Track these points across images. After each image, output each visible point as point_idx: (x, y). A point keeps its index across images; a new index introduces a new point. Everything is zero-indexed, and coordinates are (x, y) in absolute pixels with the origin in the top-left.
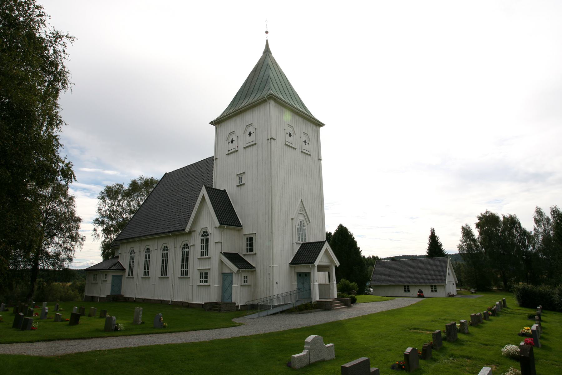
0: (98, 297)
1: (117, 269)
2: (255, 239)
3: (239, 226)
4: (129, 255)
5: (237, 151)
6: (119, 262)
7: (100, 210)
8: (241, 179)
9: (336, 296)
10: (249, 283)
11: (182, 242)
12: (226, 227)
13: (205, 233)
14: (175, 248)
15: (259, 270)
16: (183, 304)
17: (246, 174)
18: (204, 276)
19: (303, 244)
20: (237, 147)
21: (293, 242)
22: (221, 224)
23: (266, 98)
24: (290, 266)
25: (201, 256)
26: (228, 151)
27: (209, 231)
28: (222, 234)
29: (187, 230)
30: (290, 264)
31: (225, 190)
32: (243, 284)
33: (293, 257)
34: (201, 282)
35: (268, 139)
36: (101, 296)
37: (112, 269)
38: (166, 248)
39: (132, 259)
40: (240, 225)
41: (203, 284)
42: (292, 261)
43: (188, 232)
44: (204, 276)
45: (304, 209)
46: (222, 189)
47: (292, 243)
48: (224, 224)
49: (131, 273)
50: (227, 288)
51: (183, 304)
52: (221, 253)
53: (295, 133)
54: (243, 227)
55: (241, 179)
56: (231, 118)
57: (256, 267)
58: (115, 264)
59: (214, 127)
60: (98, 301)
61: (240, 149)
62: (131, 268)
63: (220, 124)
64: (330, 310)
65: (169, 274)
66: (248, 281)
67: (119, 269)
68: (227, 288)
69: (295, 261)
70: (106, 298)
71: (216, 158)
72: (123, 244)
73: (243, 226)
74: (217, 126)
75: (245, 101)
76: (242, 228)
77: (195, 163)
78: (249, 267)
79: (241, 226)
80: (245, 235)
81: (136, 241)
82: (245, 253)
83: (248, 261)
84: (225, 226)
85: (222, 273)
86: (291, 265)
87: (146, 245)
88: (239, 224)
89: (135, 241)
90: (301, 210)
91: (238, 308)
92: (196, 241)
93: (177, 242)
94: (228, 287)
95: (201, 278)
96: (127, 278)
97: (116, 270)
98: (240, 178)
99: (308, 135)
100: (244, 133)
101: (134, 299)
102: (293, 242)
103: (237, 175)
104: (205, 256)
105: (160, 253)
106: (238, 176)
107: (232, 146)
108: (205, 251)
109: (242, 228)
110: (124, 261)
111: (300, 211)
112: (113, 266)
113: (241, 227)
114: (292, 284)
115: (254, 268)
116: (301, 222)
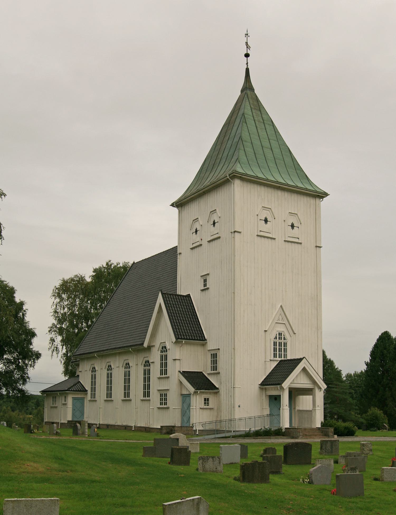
0: (59, 423)
1: (77, 390)
2: (219, 355)
3: (202, 340)
4: (90, 373)
5: (201, 245)
6: (80, 382)
7: (56, 312)
8: (205, 281)
9: (319, 425)
10: (211, 406)
11: (124, 362)
12: (184, 341)
13: (164, 349)
14: (101, 369)
15: (223, 391)
16: (146, 429)
17: (210, 275)
18: (164, 397)
19: (281, 361)
20: (201, 239)
21: (265, 359)
22: (177, 339)
23: (228, 177)
24: (260, 388)
25: (161, 375)
26: (193, 244)
27: (167, 346)
28: (181, 350)
29: (145, 345)
30: (259, 385)
31: (189, 294)
32: (203, 406)
33: (265, 377)
34: (161, 404)
35: (232, 233)
36: (61, 422)
37: (71, 391)
38: (127, 366)
39: (94, 378)
40: (204, 339)
41: (163, 406)
42: (263, 382)
43: (146, 347)
44: (164, 397)
45: (285, 318)
46: (185, 295)
47: (264, 360)
48: (181, 339)
49: (93, 395)
50: (186, 411)
51: (146, 429)
52: (180, 372)
53: (274, 216)
54: (208, 341)
55: (205, 281)
56: (194, 199)
57: (219, 388)
58: (75, 385)
59: (176, 210)
60: (59, 427)
61: (205, 243)
62: (93, 389)
63: (183, 206)
64: (297, 439)
65: (132, 396)
66: (210, 404)
67: (80, 390)
68: (186, 411)
69: (265, 383)
70: (67, 423)
71: (180, 252)
72: (83, 359)
73: (207, 340)
74: (180, 209)
75: (211, 173)
76: (206, 343)
77: (168, 249)
78: (210, 387)
79: (205, 340)
80: (209, 350)
81: (130, 352)
82: (210, 372)
83: (212, 381)
84: (183, 341)
85: (182, 395)
86: (261, 387)
87: (144, 357)
88: (202, 337)
89: (94, 357)
90: (280, 319)
91: (196, 432)
92: (155, 356)
93: (139, 359)
94: (187, 409)
95: (161, 399)
96: (90, 401)
97: (76, 391)
98: (204, 280)
99: (297, 215)
100: (208, 222)
101: (98, 425)
102: (265, 359)
103: (202, 276)
104: (165, 375)
105: (105, 372)
106: (202, 277)
107: (196, 238)
108: (164, 371)
109: (206, 343)
110: (85, 379)
111: (279, 320)
112: (72, 387)
113: (205, 342)
114: (263, 409)
115: (217, 389)
116: (280, 334)
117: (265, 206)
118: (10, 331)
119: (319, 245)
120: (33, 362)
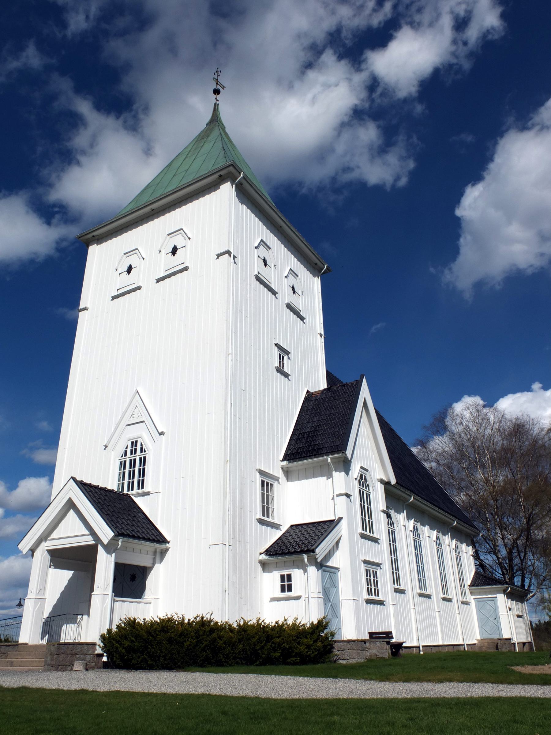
27: (365, 576)
113: (162, 546)
116: (134, 444)
117: (438, 647)
118: (179, 638)
119: (433, 643)
120: (521, 535)
